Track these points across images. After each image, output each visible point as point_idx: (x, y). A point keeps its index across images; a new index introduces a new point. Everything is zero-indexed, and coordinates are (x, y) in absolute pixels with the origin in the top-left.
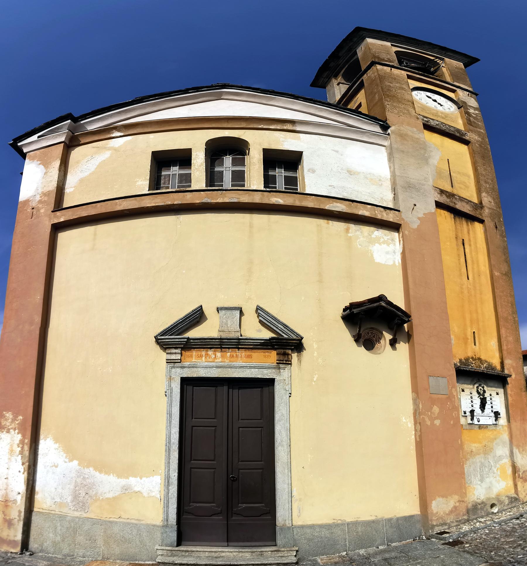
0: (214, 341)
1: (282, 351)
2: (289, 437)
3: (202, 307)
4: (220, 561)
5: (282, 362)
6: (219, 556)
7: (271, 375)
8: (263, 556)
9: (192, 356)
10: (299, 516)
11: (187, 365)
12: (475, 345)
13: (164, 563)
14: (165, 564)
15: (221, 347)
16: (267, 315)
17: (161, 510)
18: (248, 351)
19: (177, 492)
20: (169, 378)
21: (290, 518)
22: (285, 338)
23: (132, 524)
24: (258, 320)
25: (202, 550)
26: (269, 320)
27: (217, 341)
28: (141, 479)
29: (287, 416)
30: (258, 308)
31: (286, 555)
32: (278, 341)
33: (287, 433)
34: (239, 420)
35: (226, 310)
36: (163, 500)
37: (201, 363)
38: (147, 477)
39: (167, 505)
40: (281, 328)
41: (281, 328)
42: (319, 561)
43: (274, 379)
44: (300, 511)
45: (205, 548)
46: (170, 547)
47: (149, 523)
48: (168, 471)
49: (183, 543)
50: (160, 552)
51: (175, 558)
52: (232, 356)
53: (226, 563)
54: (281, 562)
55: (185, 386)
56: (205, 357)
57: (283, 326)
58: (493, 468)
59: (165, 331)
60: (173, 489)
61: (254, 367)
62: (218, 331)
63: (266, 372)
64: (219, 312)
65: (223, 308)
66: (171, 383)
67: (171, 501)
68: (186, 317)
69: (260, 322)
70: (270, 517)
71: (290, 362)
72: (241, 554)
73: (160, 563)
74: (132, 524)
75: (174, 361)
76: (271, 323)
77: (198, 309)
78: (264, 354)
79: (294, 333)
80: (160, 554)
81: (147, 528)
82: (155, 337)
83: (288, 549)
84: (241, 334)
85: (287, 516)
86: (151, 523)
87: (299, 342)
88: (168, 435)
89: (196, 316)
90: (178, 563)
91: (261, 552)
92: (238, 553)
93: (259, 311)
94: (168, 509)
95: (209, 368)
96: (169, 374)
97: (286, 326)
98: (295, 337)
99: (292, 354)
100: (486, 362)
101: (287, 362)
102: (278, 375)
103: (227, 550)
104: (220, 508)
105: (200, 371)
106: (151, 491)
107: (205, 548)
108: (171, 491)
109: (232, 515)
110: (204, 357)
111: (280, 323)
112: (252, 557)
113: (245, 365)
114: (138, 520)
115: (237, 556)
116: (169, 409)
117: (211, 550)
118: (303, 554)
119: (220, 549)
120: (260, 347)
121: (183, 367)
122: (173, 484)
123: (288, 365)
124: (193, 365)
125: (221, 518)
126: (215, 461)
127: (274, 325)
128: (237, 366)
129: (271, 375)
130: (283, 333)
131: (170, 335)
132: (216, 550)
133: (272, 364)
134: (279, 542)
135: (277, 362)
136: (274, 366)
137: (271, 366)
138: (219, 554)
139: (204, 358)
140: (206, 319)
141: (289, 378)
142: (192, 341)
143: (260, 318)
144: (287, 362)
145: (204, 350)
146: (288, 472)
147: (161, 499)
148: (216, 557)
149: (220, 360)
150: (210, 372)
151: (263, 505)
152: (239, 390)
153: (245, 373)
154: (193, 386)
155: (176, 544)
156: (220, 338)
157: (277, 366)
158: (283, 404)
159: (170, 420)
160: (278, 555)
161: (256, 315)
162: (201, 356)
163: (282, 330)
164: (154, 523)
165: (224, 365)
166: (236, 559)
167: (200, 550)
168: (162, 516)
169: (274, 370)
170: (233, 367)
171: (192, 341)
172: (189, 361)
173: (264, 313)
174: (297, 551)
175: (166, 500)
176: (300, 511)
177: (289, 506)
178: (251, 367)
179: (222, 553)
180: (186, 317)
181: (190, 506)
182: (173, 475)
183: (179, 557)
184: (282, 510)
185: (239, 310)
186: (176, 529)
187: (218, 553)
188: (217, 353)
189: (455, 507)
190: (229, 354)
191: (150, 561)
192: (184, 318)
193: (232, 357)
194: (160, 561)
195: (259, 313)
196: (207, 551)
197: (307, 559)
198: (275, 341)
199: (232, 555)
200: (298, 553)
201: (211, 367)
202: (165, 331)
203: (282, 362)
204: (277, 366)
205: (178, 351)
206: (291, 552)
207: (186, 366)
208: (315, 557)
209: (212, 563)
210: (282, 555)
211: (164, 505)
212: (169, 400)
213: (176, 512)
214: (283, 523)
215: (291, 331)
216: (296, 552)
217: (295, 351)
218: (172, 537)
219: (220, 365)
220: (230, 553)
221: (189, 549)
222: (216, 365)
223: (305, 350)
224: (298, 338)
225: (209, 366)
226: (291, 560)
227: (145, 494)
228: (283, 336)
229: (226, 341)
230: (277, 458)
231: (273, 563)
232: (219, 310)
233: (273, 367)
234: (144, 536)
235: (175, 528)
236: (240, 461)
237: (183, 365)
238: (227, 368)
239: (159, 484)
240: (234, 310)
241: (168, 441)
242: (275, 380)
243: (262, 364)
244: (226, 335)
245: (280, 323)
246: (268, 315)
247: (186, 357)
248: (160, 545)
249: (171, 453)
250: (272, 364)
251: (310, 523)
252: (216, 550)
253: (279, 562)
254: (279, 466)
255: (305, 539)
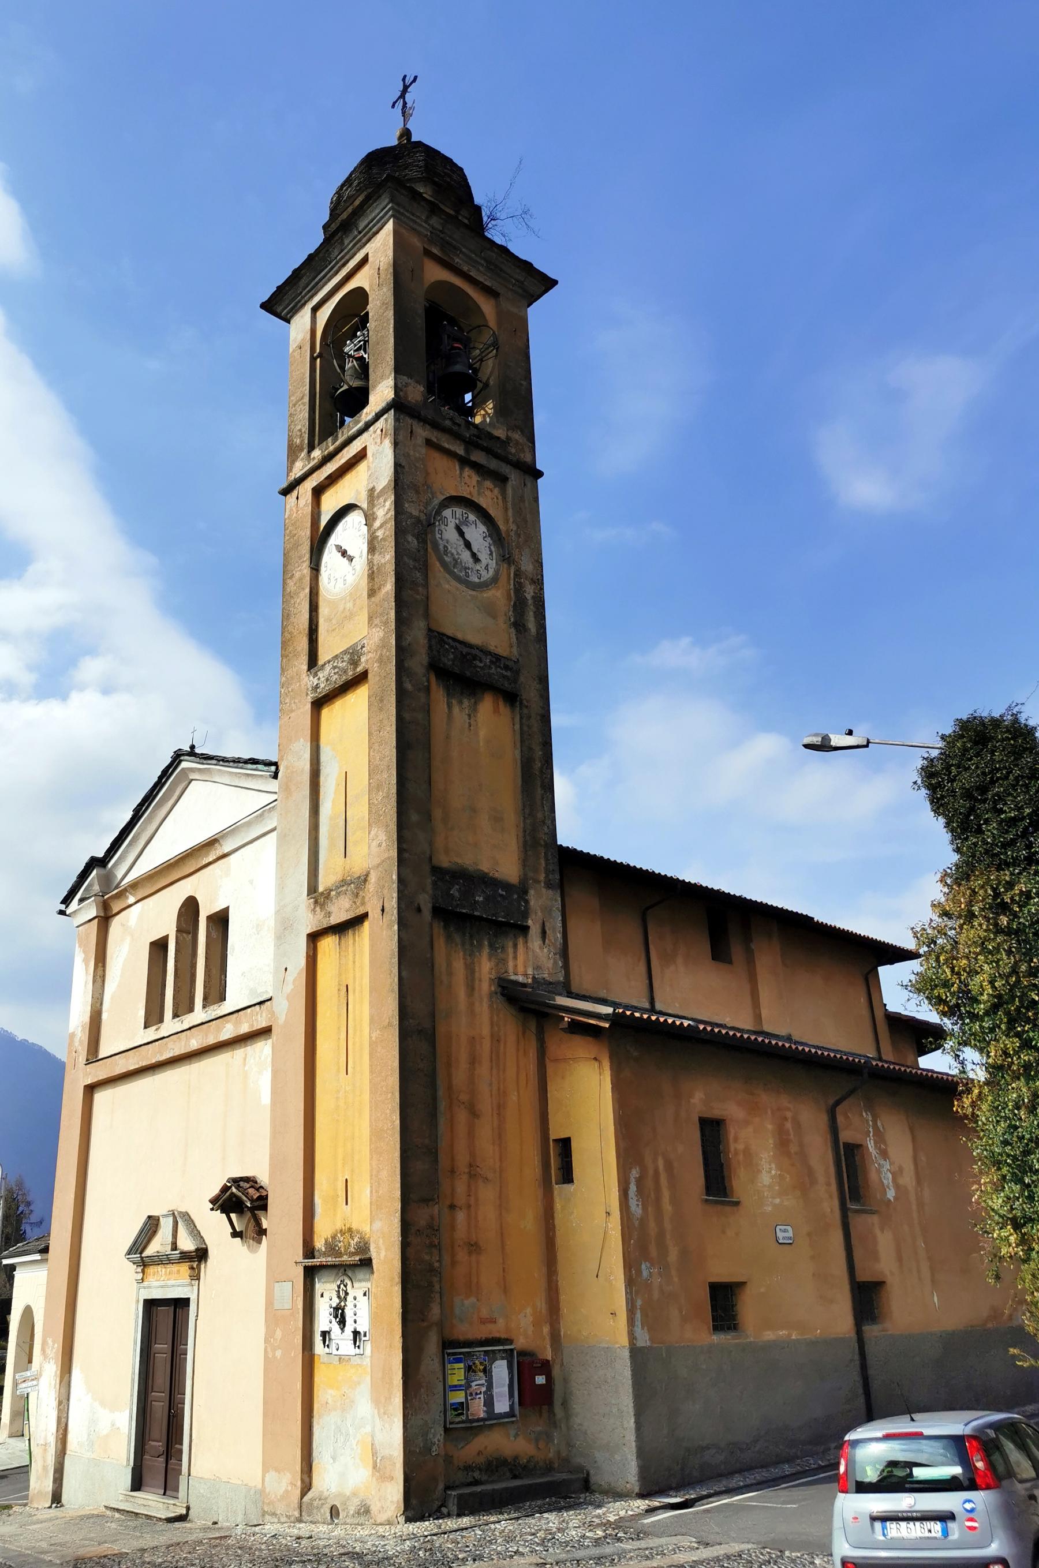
12: (347, 1204)
58: (351, 1438)
100: (358, 1232)
151: (161, 1444)
189: (286, 1491)
190: (152, 1270)
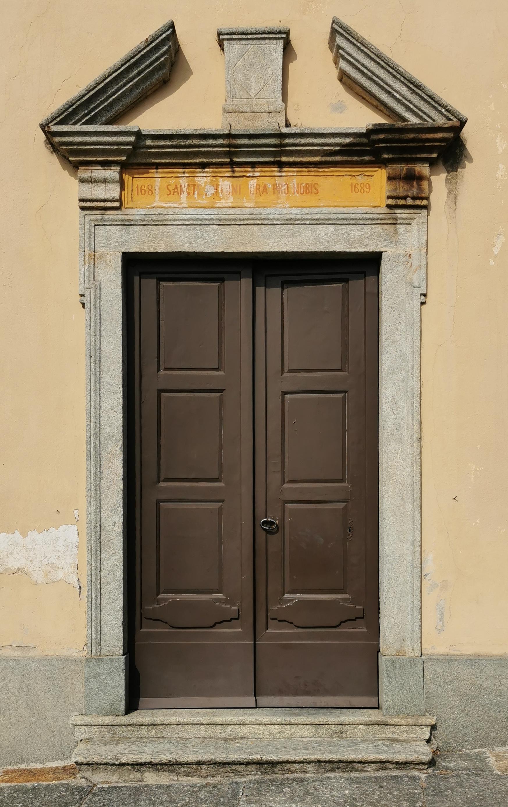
0: (211, 142)
1: (403, 168)
2: (417, 416)
3: (174, 31)
4: (235, 752)
5: (401, 202)
6: (234, 734)
7: (371, 242)
8: (344, 735)
9: (151, 191)
10: (440, 630)
11: (138, 217)
13: (92, 764)
14: (96, 767)
15: (232, 160)
16: (362, 51)
17: (82, 620)
18: (306, 174)
19: (122, 567)
20: (90, 255)
21: (417, 635)
22: (411, 125)
23: (4, 660)
24: (335, 73)
25: (191, 720)
26: (366, 68)
27: (220, 142)
28: (24, 534)
29: (414, 359)
30: (336, 27)
31: (404, 736)
32: (390, 136)
33: (413, 406)
34: (282, 373)
35: (244, 39)
36: (86, 590)
37: (177, 211)
38: (41, 530)
39: (98, 603)
40: (400, 94)
41: (400, 94)
42: (492, 760)
43: (381, 253)
44: (442, 615)
45: (198, 713)
46: (107, 718)
47: (51, 653)
48: (96, 512)
49: (143, 701)
50: (82, 733)
51: (122, 747)
52: (261, 189)
53: (251, 757)
54: (391, 758)
55: (137, 278)
56: (189, 194)
57: (407, 86)
59: (70, 110)
60: (113, 560)
61: (324, 222)
62: (221, 111)
63: (357, 233)
64: (223, 50)
65: (234, 34)
66: (96, 270)
67: (107, 590)
68: (128, 64)
69: (343, 77)
70: (364, 630)
71: (424, 202)
72: (288, 731)
73: (82, 764)
74: (4, 660)
75: (102, 204)
76: (374, 78)
77: (164, 36)
78: (354, 181)
79: (440, 108)
80: (82, 737)
81: (47, 668)
82: (43, 127)
83: (409, 720)
84: (287, 120)
85: (409, 627)
86: (57, 654)
87: (453, 138)
88: (93, 413)
89: (158, 59)
90: (129, 762)
91: (340, 726)
92: (280, 727)
93: (339, 40)
94: (101, 611)
95: (200, 225)
96: (90, 244)
97: (415, 86)
98: (440, 121)
99: (433, 178)
101: (418, 202)
102: (391, 242)
103: (252, 719)
104: (234, 605)
105: (175, 234)
106: (52, 567)
107: (198, 713)
108: (107, 565)
109: (267, 625)
110: (186, 194)
111: (399, 76)
112: (316, 740)
113: (299, 216)
114: (20, 648)
115: (278, 736)
116: (92, 343)
117: (212, 719)
118: (450, 735)
119: (235, 716)
120: (339, 158)
121: (127, 224)
122: (111, 545)
123: (419, 211)
124: (154, 217)
125: (240, 630)
126: (220, 481)
127: (382, 84)
128: (277, 220)
129: (371, 242)
130: (408, 109)
131: (86, 123)
132: (227, 718)
133: (374, 210)
134: (385, 699)
135: (390, 202)
136: (381, 216)
137: (372, 216)
138: (233, 730)
139: (184, 196)
140: (188, 72)
141: (421, 250)
142: (149, 142)
143: (343, 65)
144: (418, 202)
145: (184, 173)
146: (413, 510)
147: (80, 588)
148: (226, 740)
149: (230, 201)
150: (204, 238)
151: (347, 596)
152: (283, 288)
153: (300, 239)
154: (159, 280)
155: (122, 707)
156: (227, 132)
157: (389, 216)
158: (403, 326)
159: (98, 374)
160: (383, 736)
161: (330, 56)
162: (177, 191)
163: (404, 100)
164: (65, 653)
165: (242, 216)
166: (276, 745)
167: (185, 720)
168: (85, 632)
169: (379, 229)
170: (266, 222)
171: (149, 142)
172: (144, 206)
173: (355, 45)
174: (433, 728)
175: (93, 589)
176: (442, 615)
177: (413, 602)
178: (315, 222)
179: (242, 726)
180: (128, 64)
181: (158, 602)
182: (112, 521)
183: (132, 742)
184: (395, 613)
185: (279, 39)
186: (123, 667)
187: (232, 727)
188: (221, 179)
190: (253, 182)
191: (57, 760)
192: (122, 65)
193: (264, 191)
194: (80, 759)
195: (339, 47)
196: (203, 722)
197: (460, 750)
198: (382, 136)
199: (266, 732)
200: (436, 732)
201: (204, 222)
202: (70, 110)
203: (401, 202)
204: (389, 216)
205: (113, 173)
206: (417, 728)
207: (137, 221)
208: (480, 747)
209: (213, 757)
210: (394, 736)
211: (88, 602)
212: (93, 320)
213: (122, 620)
214: (397, 646)
215: (432, 102)
216: (429, 729)
217: (441, 167)
218: (114, 687)
219: (231, 217)
220: (262, 728)
221: (158, 719)
222: (217, 217)
223: (471, 161)
224: (449, 124)
225: (201, 220)
226: (416, 752)
227: (38, 576)
228: (404, 120)
229: (246, 141)
230: (385, 472)
231: (368, 760)
232: (223, 39)
233: (377, 220)
234: (39, 693)
235: (121, 662)
236: (287, 480)
237: (127, 217)
238: (251, 226)
239: (75, 545)
240: (267, 41)
241: (92, 432)
242: (383, 257)
243: (345, 210)
244: (246, 123)
245: (399, 76)
246: (366, 50)
247: (135, 192)
248: (84, 713)
249: (103, 463)
250: (374, 210)
251: (468, 650)
252: (227, 718)
253: (385, 757)
254: (390, 493)
255: (454, 695)
